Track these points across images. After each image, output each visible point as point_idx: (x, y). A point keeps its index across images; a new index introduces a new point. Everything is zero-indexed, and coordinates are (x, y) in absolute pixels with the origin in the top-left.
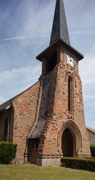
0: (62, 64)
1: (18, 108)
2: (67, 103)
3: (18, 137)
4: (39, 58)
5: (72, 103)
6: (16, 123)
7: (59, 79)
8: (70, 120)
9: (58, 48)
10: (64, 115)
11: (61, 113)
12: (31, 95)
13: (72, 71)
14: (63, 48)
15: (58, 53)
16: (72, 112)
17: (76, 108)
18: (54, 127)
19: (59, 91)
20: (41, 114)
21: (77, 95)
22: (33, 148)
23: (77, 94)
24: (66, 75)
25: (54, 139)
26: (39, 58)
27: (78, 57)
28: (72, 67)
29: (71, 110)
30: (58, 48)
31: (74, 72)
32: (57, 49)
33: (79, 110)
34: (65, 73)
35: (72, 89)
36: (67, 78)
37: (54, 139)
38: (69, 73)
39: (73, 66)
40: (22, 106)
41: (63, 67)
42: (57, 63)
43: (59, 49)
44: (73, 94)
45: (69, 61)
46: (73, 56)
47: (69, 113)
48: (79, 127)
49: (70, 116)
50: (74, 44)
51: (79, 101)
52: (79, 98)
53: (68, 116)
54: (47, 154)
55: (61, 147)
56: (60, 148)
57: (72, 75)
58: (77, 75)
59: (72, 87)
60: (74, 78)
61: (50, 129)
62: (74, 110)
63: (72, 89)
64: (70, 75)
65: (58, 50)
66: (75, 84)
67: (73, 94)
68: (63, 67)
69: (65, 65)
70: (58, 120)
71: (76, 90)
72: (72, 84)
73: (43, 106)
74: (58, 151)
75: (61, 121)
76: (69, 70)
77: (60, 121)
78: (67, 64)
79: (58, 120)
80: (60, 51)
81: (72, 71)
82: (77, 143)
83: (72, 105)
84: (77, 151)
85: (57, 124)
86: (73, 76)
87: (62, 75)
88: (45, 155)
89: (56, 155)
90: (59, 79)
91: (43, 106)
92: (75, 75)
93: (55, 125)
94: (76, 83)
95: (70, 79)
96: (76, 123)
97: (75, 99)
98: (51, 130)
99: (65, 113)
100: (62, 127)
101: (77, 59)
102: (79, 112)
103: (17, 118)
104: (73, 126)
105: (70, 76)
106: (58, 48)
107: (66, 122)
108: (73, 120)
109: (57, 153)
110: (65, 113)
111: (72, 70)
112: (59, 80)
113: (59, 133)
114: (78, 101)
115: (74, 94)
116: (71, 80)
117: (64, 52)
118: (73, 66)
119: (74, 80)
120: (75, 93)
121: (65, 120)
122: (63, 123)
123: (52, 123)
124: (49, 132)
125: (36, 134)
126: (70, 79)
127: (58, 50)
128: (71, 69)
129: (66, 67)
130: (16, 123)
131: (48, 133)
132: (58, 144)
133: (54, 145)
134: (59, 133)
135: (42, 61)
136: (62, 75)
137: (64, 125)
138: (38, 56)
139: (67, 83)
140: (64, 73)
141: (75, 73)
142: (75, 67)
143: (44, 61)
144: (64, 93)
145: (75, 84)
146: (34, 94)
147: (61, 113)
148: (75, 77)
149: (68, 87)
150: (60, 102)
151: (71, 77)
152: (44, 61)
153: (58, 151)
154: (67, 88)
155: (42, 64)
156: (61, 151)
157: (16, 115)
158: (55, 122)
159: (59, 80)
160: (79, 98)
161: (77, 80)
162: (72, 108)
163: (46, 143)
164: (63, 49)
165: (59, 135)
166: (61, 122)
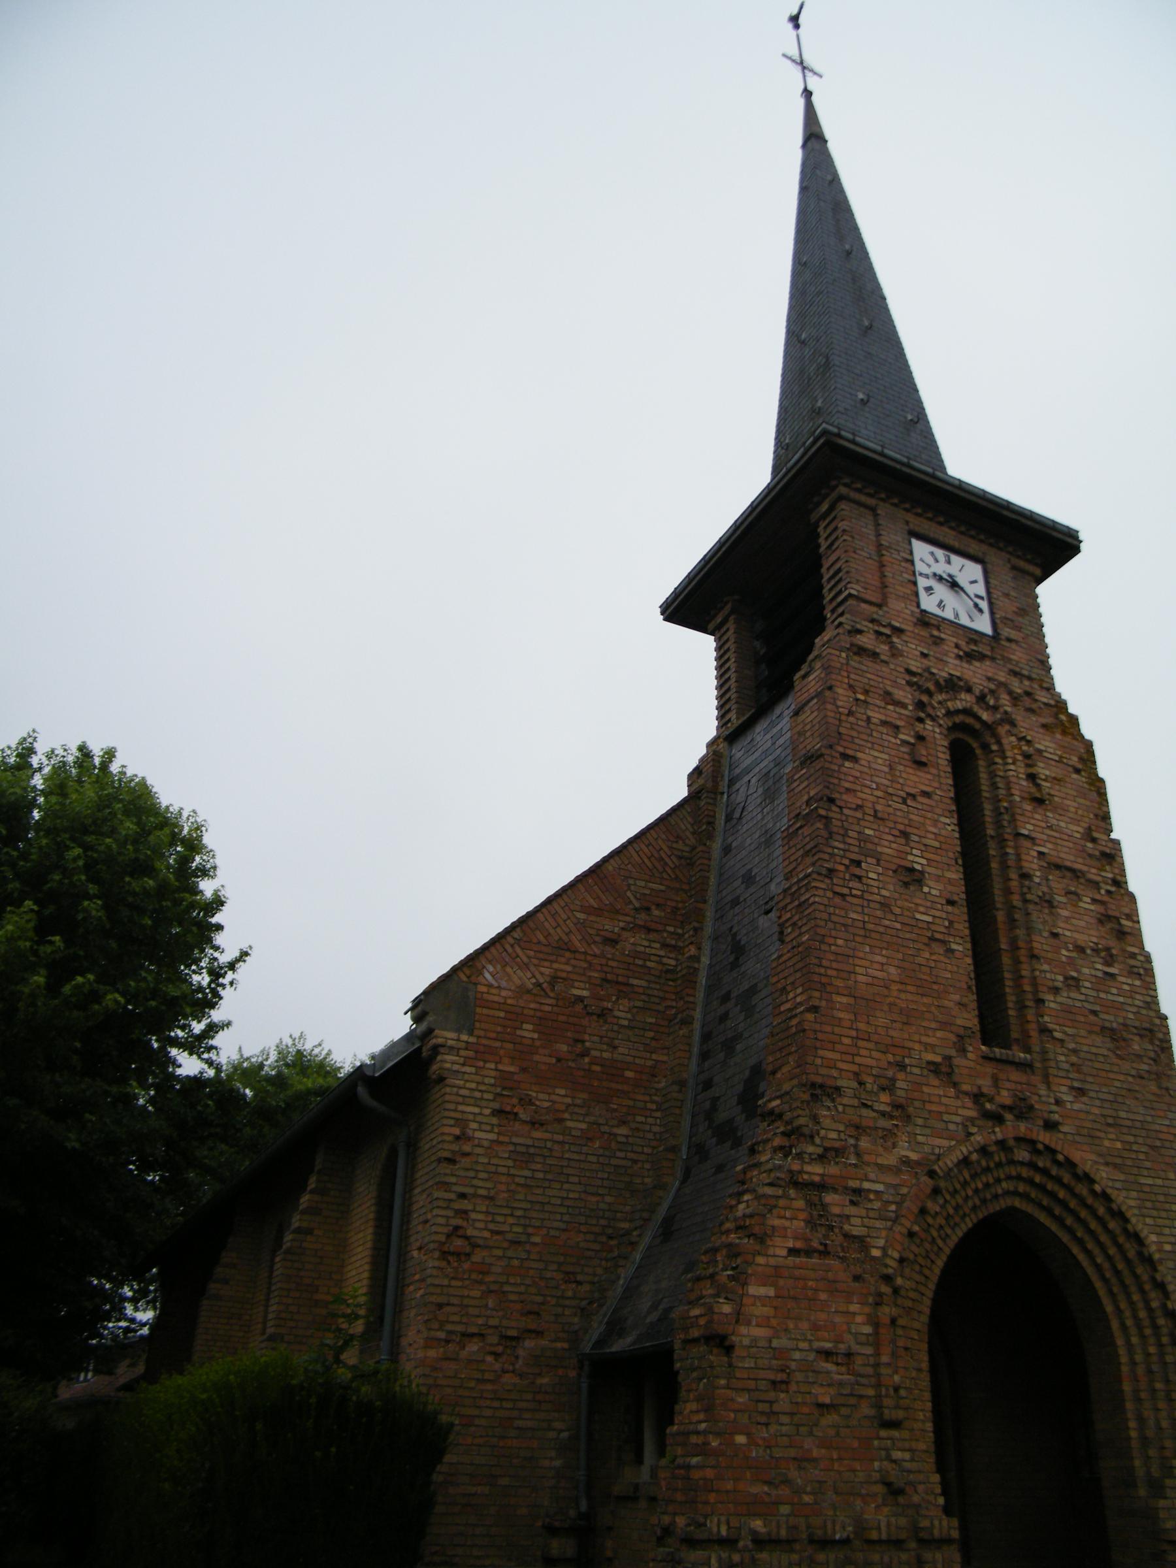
0: (864, 625)
1: (480, 1054)
2: (956, 965)
3: (473, 1347)
4: (687, 607)
5: (1017, 962)
6: (463, 1196)
7: (845, 757)
8: (1012, 1128)
9: (825, 507)
10: (934, 1088)
11: (902, 1067)
12: (610, 926)
13: (976, 674)
14: (863, 498)
15: (824, 545)
16: (1027, 1049)
17: (1067, 1010)
18: (819, 1217)
19: (858, 864)
20: (715, 1100)
21: (1058, 884)
22: (639, 1461)
23: (1058, 867)
24: (920, 705)
25: (827, 1354)
26: (687, 607)
27: (1043, 546)
28: (974, 636)
29: (1015, 1035)
30: (819, 504)
31: (1002, 676)
32: (814, 517)
33: (1110, 1019)
34: (905, 695)
35: (998, 824)
36: (936, 732)
37: (827, 1354)
38: (952, 685)
39: (983, 624)
40: (528, 1031)
41: (883, 649)
42: (825, 619)
43: (832, 508)
44: (1013, 875)
45: (949, 585)
46: (974, 547)
47: (989, 1069)
48: (1127, 1201)
49: (1005, 1097)
50: (975, 450)
51: (1090, 936)
52: (1086, 904)
53: (978, 1097)
54: (758, 1524)
55: (926, 1443)
56: (913, 1451)
57: (981, 699)
58: (1043, 697)
59: (998, 813)
60: (1013, 724)
61: (779, 1248)
62: (1044, 1031)
63: (998, 824)
64: (965, 700)
65: (824, 516)
66: (1032, 777)
67: (1013, 875)
68: (883, 649)
69: (899, 631)
70: (864, 1143)
71: (1045, 835)
72: (994, 786)
73: (724, 1018)
74: (894, 1491)
75: (904, 1150)
76: (953, 667)
77: (890, 1160)
78: (925, 620)
79: (864, 1143)
80: (842, 525)
81: (976, 674)
82: (1127, 1387)
83: (1018, 978)
84: (1142, 1492)
85: (858, 1191)
86: (995, 708)
87: (876, 716)
88: (729, 1543)
89: (921, 1541)
90: (845, 757)
91: (724, 1018)
92: (1015, 699)
93: (829, 1198)
94: (1042, 770)
95: (969, 747)
96: (1085, 1158)
97: (1039, 917)
98: (793, 1252)
99: (943, 1071)
100: (923, 1211)
101: (1014, 568)
102: (1100, 1045)
103: (467, 1148)
104: (1052, 1195)
105: (966, 712)
106: (825, 507)
107: (965, 1161)
108: (1044, 1137)
109: (883, 1519)
110: (943, 1071)
111: (982, 657)
112: (855, 759)
113: (887, 1279)
114: (1082, 939)
115: (1025, 876)
116: (985, 747)
117: (877, 525)
118: (983, 624)
119: (1009, 741)
120: (1032, 864)
121: (944, 1131)
122: (932, 1174)
123: (796, 1184)
124: (774, 1275)
125: (654, 1307)
126: (969, 747)
127: (824, 516)
128: (969, 657)
129: (912, 651)
130: (463, 1196)
131: (753, 1290)
132: (888, 1414)
133: (831, 1419)
134: (887, 1279)
135: (711, 626)
136: (876, 716)
137: (936, 1191)
138: (676, 594)
139: (938, 780)
140: (899, 694)
141: (1017, 686)
142: (1006, 632)
143: (731, 625)
144: (912, 878)
145: (1032, 777)
146: (642, 918)
147: (902, 1067)
148: (1019, 716)
149: (960, 812)
150: (874, 966)
151: (978, 719)
152: (731, 625)
153: (894, 1491)
154: (948, 826)
155: (718, 649)
156: (928, 1489)
157: (462, 1123)
158: (833, 1170)
159: (855, 759)
160: (1086, 904)
161: (1046, 743)
162: (1022, 1007)
163: (742, 1399)
164: (871, 502)
165: (886, 1311)
166: (906, 1161)
